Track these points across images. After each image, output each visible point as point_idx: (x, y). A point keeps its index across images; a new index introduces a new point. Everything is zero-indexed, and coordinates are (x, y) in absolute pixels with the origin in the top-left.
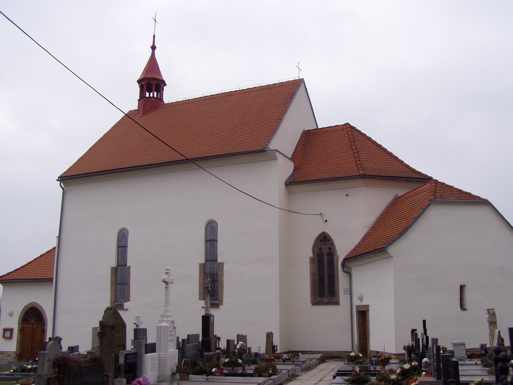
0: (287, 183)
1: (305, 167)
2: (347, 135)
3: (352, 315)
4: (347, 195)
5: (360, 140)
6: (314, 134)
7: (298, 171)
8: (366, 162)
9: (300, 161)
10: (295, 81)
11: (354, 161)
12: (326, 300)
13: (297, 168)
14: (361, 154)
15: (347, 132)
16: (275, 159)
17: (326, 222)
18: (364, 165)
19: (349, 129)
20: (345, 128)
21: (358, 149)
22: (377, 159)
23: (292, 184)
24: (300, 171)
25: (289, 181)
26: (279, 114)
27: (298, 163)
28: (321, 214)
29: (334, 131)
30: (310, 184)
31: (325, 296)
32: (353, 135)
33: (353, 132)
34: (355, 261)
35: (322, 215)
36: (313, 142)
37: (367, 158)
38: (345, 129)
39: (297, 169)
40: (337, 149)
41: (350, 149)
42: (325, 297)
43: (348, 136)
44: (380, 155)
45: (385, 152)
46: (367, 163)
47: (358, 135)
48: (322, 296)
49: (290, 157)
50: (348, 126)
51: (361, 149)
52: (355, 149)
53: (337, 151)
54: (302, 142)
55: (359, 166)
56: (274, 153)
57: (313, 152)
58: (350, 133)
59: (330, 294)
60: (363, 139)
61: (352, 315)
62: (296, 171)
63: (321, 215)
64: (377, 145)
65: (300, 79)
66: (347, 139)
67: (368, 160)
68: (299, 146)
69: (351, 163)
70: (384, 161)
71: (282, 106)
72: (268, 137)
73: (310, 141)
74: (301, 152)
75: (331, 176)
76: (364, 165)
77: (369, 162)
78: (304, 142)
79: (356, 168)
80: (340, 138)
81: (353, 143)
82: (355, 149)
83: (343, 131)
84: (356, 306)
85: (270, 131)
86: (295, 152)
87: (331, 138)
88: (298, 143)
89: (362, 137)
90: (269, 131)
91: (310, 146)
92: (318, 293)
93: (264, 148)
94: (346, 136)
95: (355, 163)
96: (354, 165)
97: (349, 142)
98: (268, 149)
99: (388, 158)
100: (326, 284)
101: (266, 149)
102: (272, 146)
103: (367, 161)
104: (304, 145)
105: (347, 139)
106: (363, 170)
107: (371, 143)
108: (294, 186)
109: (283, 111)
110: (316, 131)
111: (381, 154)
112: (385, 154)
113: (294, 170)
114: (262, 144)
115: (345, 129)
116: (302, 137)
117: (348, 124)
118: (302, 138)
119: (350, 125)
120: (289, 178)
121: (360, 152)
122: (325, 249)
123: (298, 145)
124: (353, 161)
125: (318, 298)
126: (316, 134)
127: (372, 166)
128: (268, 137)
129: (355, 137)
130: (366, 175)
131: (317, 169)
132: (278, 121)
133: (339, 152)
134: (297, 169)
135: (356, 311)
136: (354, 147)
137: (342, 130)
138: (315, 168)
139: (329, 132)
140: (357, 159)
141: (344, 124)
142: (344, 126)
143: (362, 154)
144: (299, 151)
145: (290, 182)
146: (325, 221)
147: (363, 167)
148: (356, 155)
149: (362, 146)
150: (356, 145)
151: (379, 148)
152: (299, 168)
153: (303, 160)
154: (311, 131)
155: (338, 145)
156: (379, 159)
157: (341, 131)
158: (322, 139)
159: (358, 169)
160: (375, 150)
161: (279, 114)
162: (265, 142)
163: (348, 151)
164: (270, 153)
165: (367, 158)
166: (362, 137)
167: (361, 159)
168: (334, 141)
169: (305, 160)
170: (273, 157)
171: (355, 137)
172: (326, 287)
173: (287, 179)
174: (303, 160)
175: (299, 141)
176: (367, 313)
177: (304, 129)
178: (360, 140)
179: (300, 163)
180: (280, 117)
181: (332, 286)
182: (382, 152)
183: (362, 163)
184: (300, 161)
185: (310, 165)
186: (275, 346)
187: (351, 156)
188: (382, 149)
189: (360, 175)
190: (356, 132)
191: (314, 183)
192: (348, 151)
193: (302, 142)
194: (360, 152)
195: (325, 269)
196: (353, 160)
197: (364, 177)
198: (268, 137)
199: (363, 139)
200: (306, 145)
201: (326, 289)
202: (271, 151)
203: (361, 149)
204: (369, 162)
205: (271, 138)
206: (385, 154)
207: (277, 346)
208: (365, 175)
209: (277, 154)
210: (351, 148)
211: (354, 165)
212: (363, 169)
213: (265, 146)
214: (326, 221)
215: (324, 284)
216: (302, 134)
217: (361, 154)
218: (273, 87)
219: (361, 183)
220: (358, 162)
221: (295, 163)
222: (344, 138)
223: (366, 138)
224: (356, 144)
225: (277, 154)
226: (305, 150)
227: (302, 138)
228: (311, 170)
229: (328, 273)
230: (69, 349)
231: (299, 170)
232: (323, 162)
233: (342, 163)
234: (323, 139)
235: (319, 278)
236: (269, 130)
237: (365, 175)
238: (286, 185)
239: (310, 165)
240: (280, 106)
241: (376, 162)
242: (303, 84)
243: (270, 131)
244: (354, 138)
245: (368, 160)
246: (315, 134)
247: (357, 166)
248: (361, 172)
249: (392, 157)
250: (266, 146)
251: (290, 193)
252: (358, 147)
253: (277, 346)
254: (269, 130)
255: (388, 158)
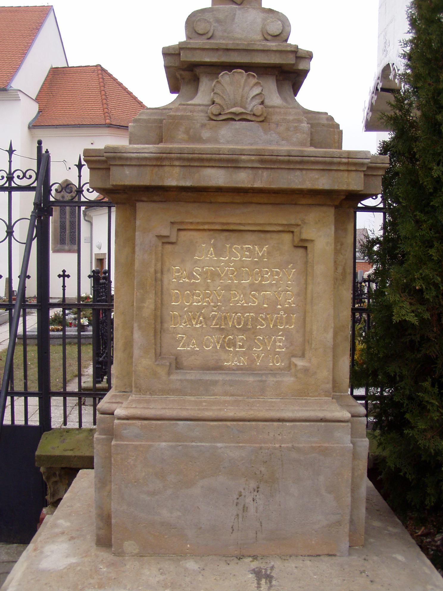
0: (31, 126)
1: (51, 110)
2: (98, 79)
3: (91, 263)
4: (92, 144)
5: (110, 85)
6: (62, 73)
7: (43, 114)
8: (114, 110)
9: (46, 102)
10: (43, 8)
11: (102, 108)
12: (66, 247)
13: (42, 111)
14: (110, 101)
15: (98, 75)
16: (18, 99)
17: (70, 170)
18: (112, 113)
19: (100, 72)
20: (96, 70)
21: (107, 95)
22: (126, 107)
23: (35, 127)
24: (45, 114)
25: (32, 125)
26: (23, 47)
27: (43, 104)
28: (64, 161)
29: (84, 72)
30: (54, 129)
31: (66, 243)
32: (103, 79)
33: (104, 75)
34: (94, 210)
35: (66, 161)
36: (61, 82)
37: (116, 106)
38: (96, 71)
39: (41, 111)
40: (86, 93)
41: (99, 94)
42: (65, 244)
43: (99, 79)
44: (130, 104)
45: (135, 101)
46: (115, 112)
47: (109, 79)
48: (63, 244)
49: (34, 98)
50: (99, 68)
51: (110, 95)
52: (104, 95)
53: (85, 95)
54: (49, 81)
55: (107, 114)
56: (17, 94)
57: (60, 94)
58: (100, 76)
59: (71, 242)
60: (114, 84)
61: (91, 263)
62: (41, 113)
63: (64, 162)
64: (127, 93)
65: (49, 6)
66: (97, 82)
67: (116, 108)
68: (46, 85)
69: (99, 110)
70: (132, 110)
71: (27, 38)
72: (11, 73)
73: (58, 81)
74: (47, 93)
75: (77, 123)
76: (112, 113)
77: (117, 110)
78: (51, 81)
79: (103, 116)
80: (90, 81)
81: (102, 88)
82: (104, 95)
83: (93, 73)
84: (95, 254)
85: (12, 67)
86: (38, 95)
87: (81, 79)
88: (44, 82)
89: (113, 82)
90: (12, 66)
91: (57, 86)
92: (59, 241)
93: (6, 87)
94: (96, 79)
95: (102, 110)
96: (101, 112)
97: (98, 86)
98: (10, 88)
99: (138, 107)
100: (67, 232)
101: (8, 88)
102: (16, 84)
103: (115, 109)
104: (51, 85)
105: (97, 82)
106: (109, 118)
107: (122, 89)
108: (37, 130)
109: (28, 45)
110: (65, 69)
111: (131, 102)
112: (134, 103)
113: (39, 112)
114: (3, 82)
115: (96, 71)
116: (49, 75)
117: (100, 66)
118: (45, 84)
119: (101, 67)
120: (32, 120)
121: (109, 99)
122: (67, 196)
123: (44, 84)
124: (101, 108)
125: (59, 246)
126: (65, 73)
127: (120, 115)
128: (10, 74)
129: (106, 81)
130: (112, 125)
131: (62, 114)
132: (22, 55)
133: (87, 97)
134: (41, 111)
135: (95, 259)
136: (103, 93)
137: (92, 72)
138: (61, 112)
139: (78, 72)
140: (105, 106)
141: (95, 65)
142: (95, 68)
143: (111, 101)
144: (45, 91)
145: (33, 126)
146: (68, 169)
147: (110, 115)
148: (104, 101)
149: (111, 91)
150: (106, 91)
151: (129, 96)
152: (44, 110)
153: (49, 102)
154: (59, 69)
155: (87, 89)
156: (128, 108)
157: (92, 73)
158: (70, 80)
159: (105, 117)
160: (125, 98)
161: (23, 47)
162: (6, 80)
163: (96, 96)
164: (12, 92)
165: (116, 106)
166: (113, 82)
167: (109, 107)
168: (83, 83)
169: (51, 102)
170: (16, 97)
171: (106, 81)
172: (67, 235)
173: (31, 122)
174: (49, 102)
175: (46, 80)
176: (104, 261)
177: (52, 66)
178: (110, 85)
179: (45, 104)
180: (24, 51)
181: (73, 234)
182: (132, 101)
183: (109, 111)
184: (46, 102)
185: (56, 108)
186: (14, 291)
187: (100, 102)
188: (132, 97)
189: (106, 124)
190: (107, 75)
191: (59, 128)
192: (96, 96)
193: (49, 81)
194: (109, 99)
195: (67, 217)
196: (100, 106)
197: (110, 126)
198: (10, 74)
199: (114, 84)
200: (53, 85)
201: (67, 237)
202: (13, 91)
203: (110, 95)
204: (117, 110)
205: (14, 75)
206: (134, 103)
207: (16, 291)
208: (111, 124)
209: (20, 95)
210: (100, 93)
211: (101, 112)
212: (110, 118)
213: (7, 85)
214: (70, 168)
215: (65, 232)
216: (49, 72)
217: (110, 101)
218: (16, 11)
219: (107, 132)
220: (106, 110)
221: (40, 105)
222: (94, 81)
223: (117, 83)
224: (106, 89)
225: (20, 95)
226: (52, 91)
227: (45, 84)
228: (56, 114)
229: (70, 221)
230: (295, 51)
231: (44, 112)
232: (70, 105)
233: (90, 109)
234: (72, 80)
235: (61, 226)
236: (11, 65)
237: (111, 124)
238: (29, 128)
239: (56, 108)
240: (25, 37)
241: (124, 111)
242: (52, 12)
243: (12, 67)
244: (105, 83)
245: (116, 108)
246: (63, 73)
247: (104, 114)
248: (108, 121)
249: (141, 107)
250: (8, 84)
251: (33, 137)
252: (107, 93)
253: (16, 291)
254: (11, 65)
255: (138, 107)
